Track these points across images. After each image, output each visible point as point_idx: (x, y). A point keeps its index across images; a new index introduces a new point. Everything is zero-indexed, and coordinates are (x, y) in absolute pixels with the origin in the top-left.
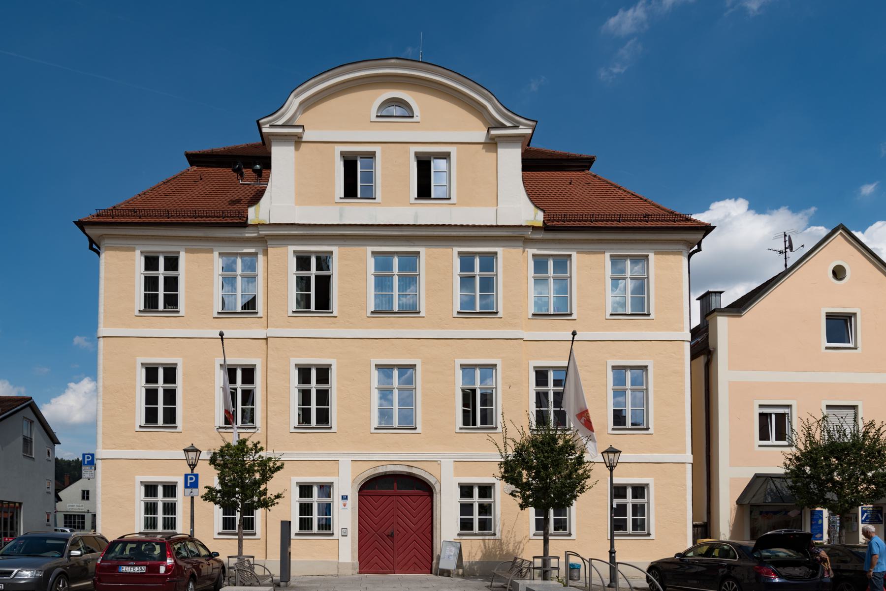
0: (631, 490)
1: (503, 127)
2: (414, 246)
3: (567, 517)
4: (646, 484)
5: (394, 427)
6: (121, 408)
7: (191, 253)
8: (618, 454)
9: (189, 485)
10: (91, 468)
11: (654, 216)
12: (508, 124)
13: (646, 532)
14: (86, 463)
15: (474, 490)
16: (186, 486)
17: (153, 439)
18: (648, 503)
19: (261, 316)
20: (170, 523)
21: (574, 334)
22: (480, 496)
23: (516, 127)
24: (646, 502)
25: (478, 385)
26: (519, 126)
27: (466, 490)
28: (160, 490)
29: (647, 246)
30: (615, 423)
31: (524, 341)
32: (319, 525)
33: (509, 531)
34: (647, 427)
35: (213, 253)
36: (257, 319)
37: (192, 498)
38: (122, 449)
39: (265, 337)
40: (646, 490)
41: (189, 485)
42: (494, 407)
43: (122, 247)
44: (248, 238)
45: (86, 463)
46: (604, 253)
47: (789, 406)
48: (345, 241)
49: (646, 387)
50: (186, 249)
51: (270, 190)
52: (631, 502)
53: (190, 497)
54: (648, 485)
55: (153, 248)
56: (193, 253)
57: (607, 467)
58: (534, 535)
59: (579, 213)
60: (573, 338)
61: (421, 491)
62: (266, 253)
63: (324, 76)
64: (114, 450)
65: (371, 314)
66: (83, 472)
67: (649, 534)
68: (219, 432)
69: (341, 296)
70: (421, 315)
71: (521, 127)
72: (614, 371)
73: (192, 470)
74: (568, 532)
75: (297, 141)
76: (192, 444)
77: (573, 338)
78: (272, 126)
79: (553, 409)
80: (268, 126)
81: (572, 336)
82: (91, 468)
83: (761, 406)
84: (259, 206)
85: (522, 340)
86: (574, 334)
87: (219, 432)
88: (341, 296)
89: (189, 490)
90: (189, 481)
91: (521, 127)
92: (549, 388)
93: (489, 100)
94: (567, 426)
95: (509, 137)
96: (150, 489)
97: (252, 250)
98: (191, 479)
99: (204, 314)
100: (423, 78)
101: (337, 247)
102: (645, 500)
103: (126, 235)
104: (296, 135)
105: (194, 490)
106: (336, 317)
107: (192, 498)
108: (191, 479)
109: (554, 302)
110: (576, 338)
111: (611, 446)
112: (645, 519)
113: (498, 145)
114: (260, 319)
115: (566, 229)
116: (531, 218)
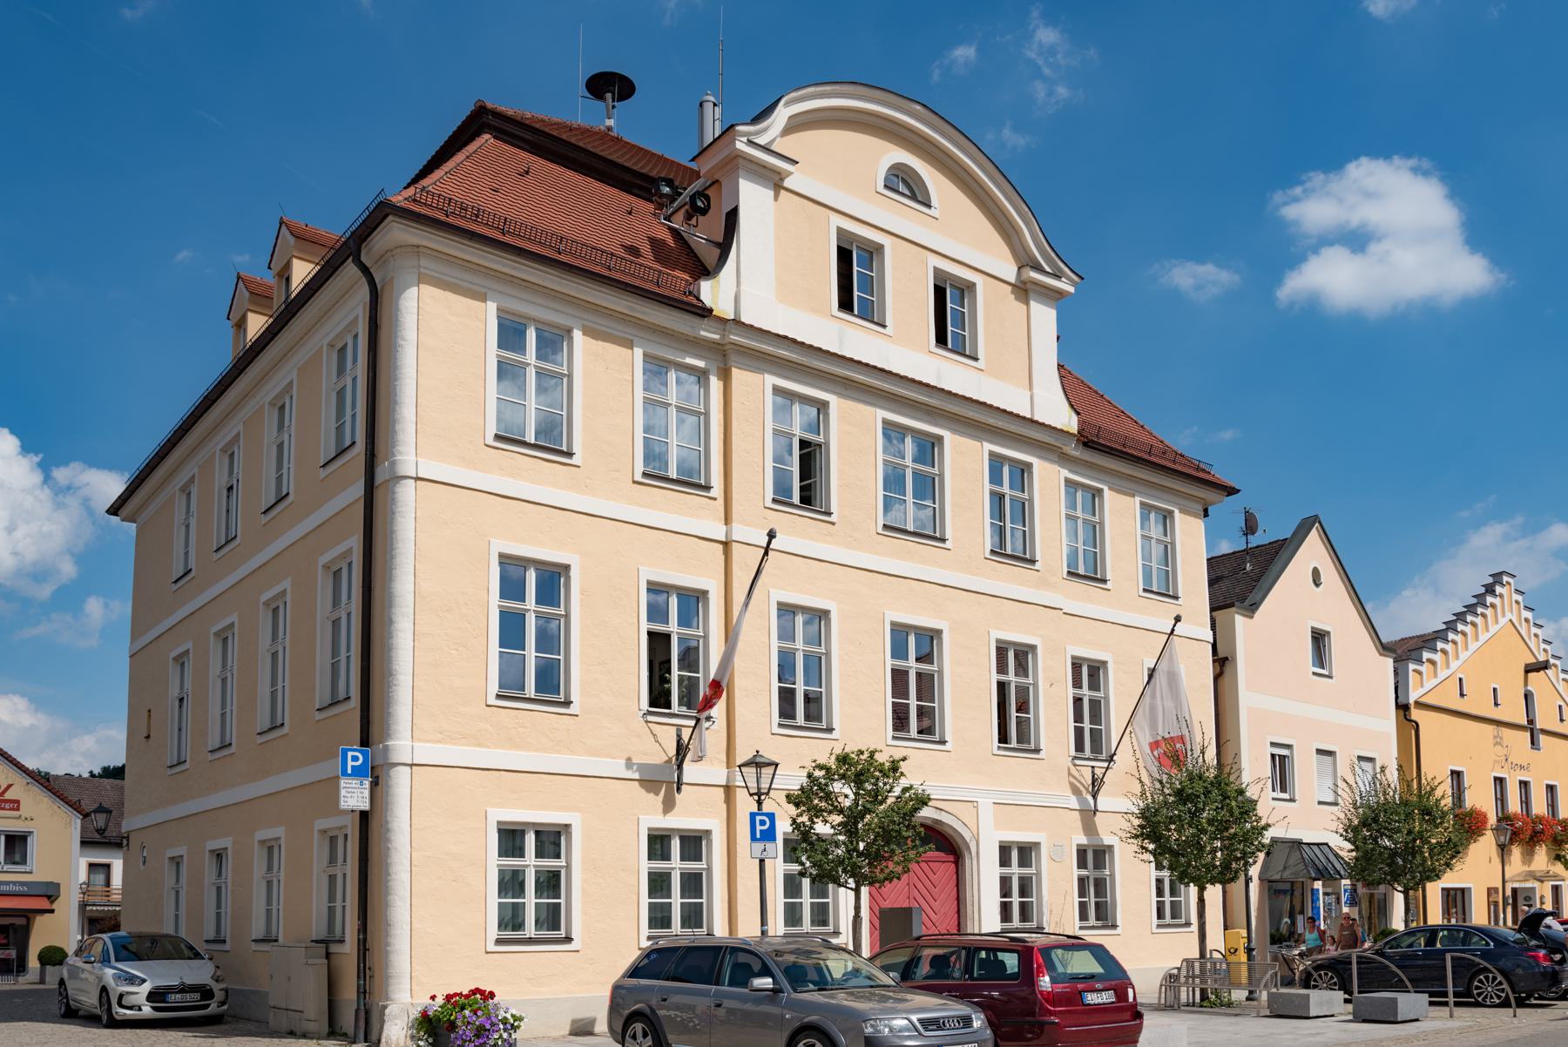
0: (533, 836)
1: (1042, 271)
2: (936, 425)
3: (703, 900)
4: (1035, 843)
5: (527, 696)
6: (457, 650)
7: (592, 338)
8: (770, 770)
9: (758, 836)
10: (361, 784)
11: (499, 219)
12: (1048, 269)
13: (562, 933)
14: (349, 771)
15: (1013, 853)
16: (753, 838)
17: (521, 727)
18: (568, 867)
19: (715, 496)
20: (693, 916)
21: (771, 535)
22: (539, 854)
23: (1057, 277)
24: (703, 869)
25: (673, 627)
26: (1060, 277)
27: (1005, 850)
28: (530, 840)
29: (1103, 477)
30: (895, 728)
31: (1064, 613)
32: (537, 922)
33: (1057, 923)
34: (565, 697)
35: (485, 302)
36: (707, 500)
37: (762, 861)
38: (455, 744)
39: (724, 540)
40: (704, 843)
41: (758, 836)
42: (1031, 716)
43: (456, 284)
44: (704, 340)
45: (349, 771)
46: (1134, 497)
47: (1289, 747)
48: (846, 389)
49: (566, 611)
50: (583, 325)
51: (735, 258)
52: (679, 868)
53: (758, 860)
54: (567, 826)
55: (523, 306)
56: (597, 340)
57: (751, 795)
58: (499, 942)
59: (454, 197)
60: (769, 543)
61: (942, 854)
62: (725, 376)
63: (828, 88)
64: (439, 746)
65: (883, 530)
66: (343, 792)
67: (568, 939)
68: (647, 722)
69: (841, 486)
70: (574, 461)
71: (1063, 279)
72: (650, 594)
73: (759, 803)
74: (831, 928)
75: (776, 182)
76: (757, 752)
77: (769, 543)
78: (751, 143)
79: (534, 654)
80: (745, 139)
81: (767, 538)
82: (361, 784)
83: (1273, 744)
84: (719, 281)
85: (1061, 612)
86: (771, 535)
87: (647, 722)
88: (841, 486)
89: (759, 846)
90: (759, 828)
91: (1063, 279)
92: (528, 607)
93: (1027, 224)
94: (562, 695)
95: (1045, 287)
96: (511, 839)
97: (701, 364)
98: (763, 823)
99: (618, 471)
100: (901, 123)
101: (835, 397)
102: (562, 862)
103: (470, 262)
104: (779, 173)
105: (769, 846)
106: (833, 524)
107: (762, 861)
108: (763, 823)
109: (1068, 555)
110: (1179, 629)
111: (815, 761)
112: (702, 903)
113: (1031, 295)
114: (712, 501)
115: (1108, 450)
116: (1066, 421)
